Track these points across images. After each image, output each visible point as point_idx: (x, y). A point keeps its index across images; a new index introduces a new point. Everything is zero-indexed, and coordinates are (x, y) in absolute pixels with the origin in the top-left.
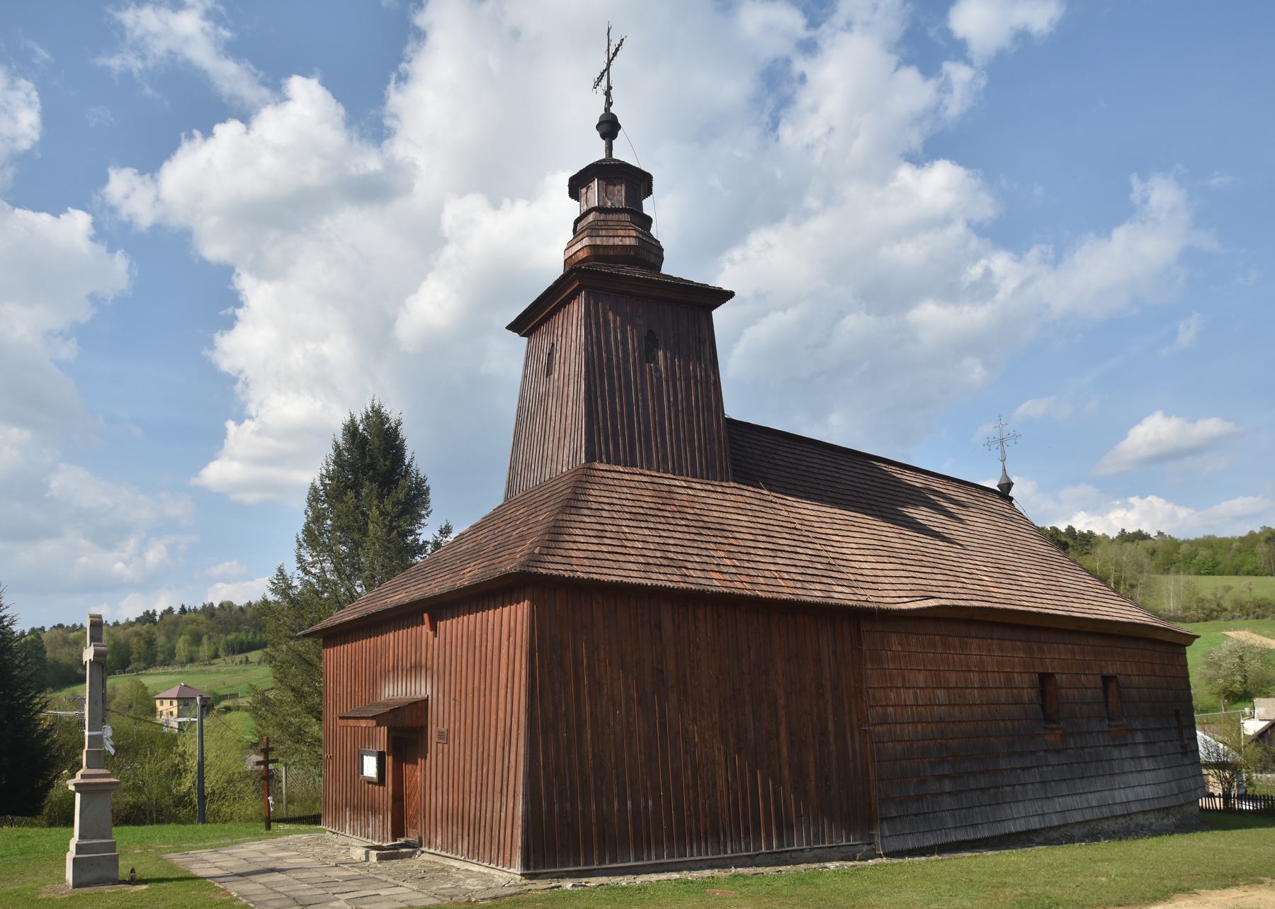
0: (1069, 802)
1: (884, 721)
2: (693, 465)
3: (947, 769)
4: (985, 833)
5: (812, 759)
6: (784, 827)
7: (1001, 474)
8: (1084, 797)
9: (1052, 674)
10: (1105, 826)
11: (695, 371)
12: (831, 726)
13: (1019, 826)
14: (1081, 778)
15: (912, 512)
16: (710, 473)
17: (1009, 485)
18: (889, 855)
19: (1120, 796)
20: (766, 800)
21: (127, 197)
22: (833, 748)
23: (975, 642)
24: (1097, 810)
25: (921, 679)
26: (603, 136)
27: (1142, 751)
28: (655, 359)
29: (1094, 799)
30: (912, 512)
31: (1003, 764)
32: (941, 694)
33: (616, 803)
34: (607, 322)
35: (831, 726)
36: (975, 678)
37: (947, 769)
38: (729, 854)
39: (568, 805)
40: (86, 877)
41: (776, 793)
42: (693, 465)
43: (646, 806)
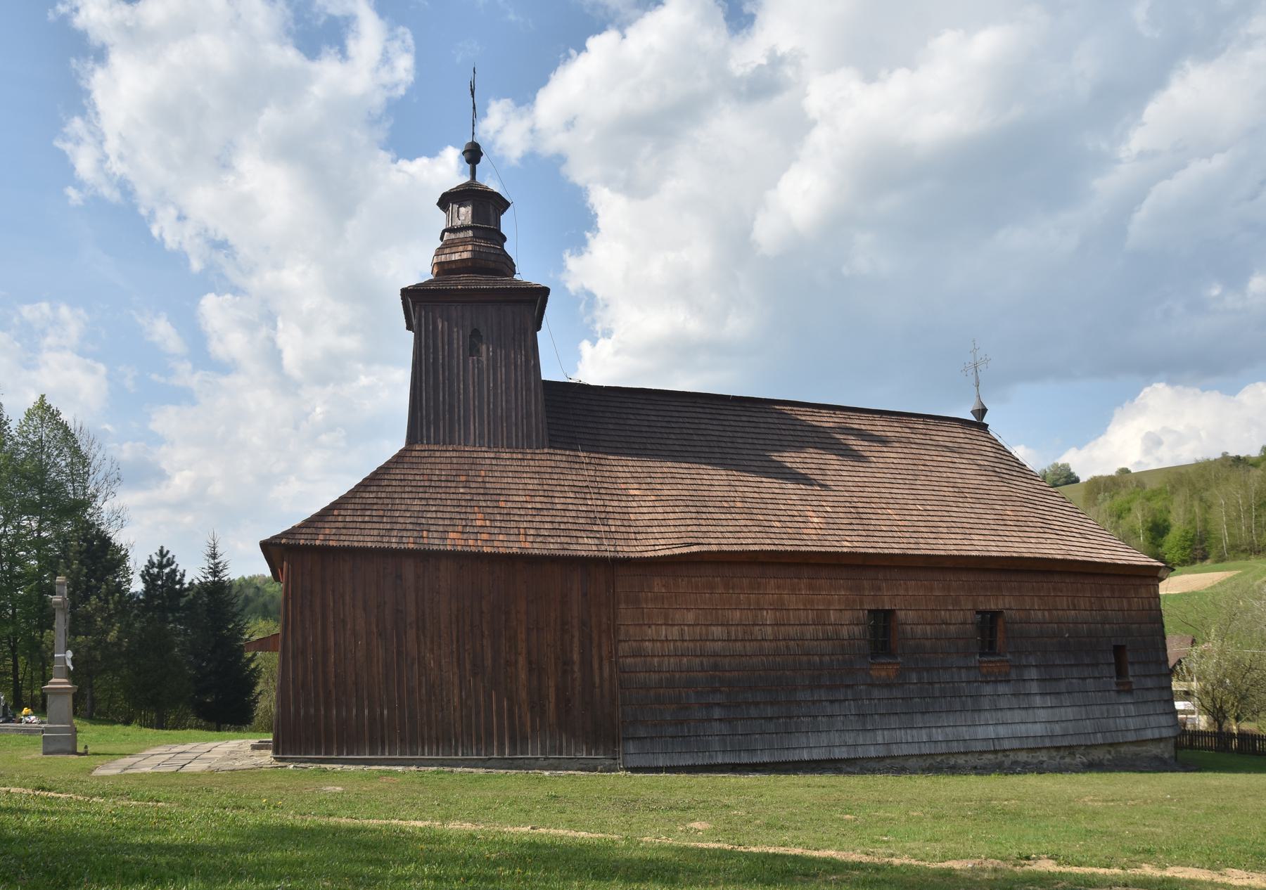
0: (900, 735)
1: (636, 654)
2: (509, 438)
3: (718, 698)
4: (766, 758)
5: (552, 683)
6: (518, 739)
7: (975, 399)
8: (924, 731)
9: (892, 612)
10: (961, 760)
11: (515, 358)
12: (576, 657)
13: (817, 755)
14: (923, 713)
15: (790, 459)
16: (524, 441)
17: (982, 412)
18: (627, 769)
19: (981, 732)
20: (500, 716)
21: (498, 132)
22: (577, 675)
23: (772, 581)
24: (944, 745)
25: (690, 617)
26: (468, 162)
27: (1034, 687)
28: (478, 352)
29: (938, 735)
30: (790, 459)
31: (801, 696)
32: (717, 631)
33: (366, 712)
34: (435, 327)
35: (576, 657)
36: (768, 616)
37: (718, 698)
38: (460, 757)
39: (312, 711)
40: (51, 748)
41: (511, 711)
42: (509, 438)
43: (382, 714)
